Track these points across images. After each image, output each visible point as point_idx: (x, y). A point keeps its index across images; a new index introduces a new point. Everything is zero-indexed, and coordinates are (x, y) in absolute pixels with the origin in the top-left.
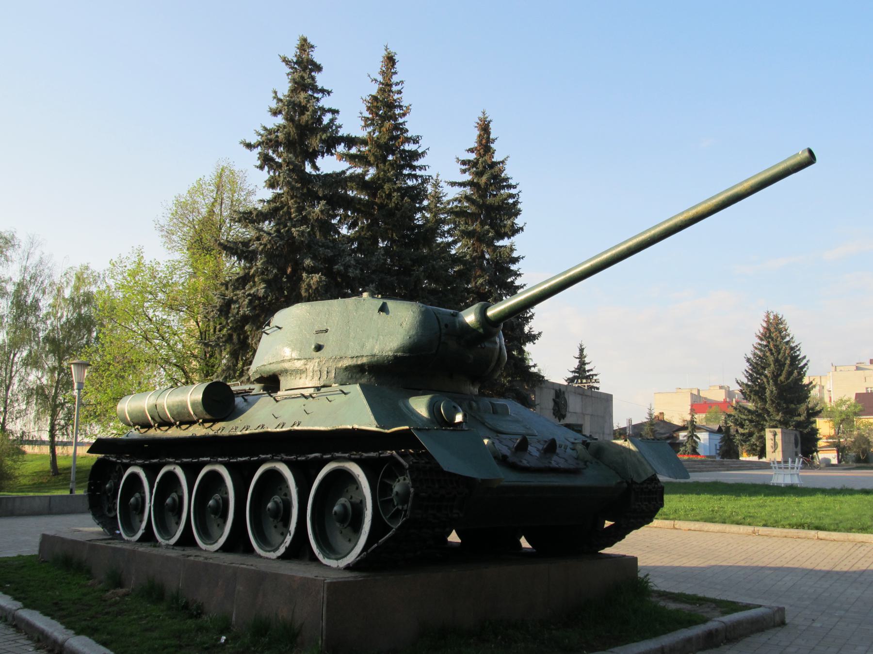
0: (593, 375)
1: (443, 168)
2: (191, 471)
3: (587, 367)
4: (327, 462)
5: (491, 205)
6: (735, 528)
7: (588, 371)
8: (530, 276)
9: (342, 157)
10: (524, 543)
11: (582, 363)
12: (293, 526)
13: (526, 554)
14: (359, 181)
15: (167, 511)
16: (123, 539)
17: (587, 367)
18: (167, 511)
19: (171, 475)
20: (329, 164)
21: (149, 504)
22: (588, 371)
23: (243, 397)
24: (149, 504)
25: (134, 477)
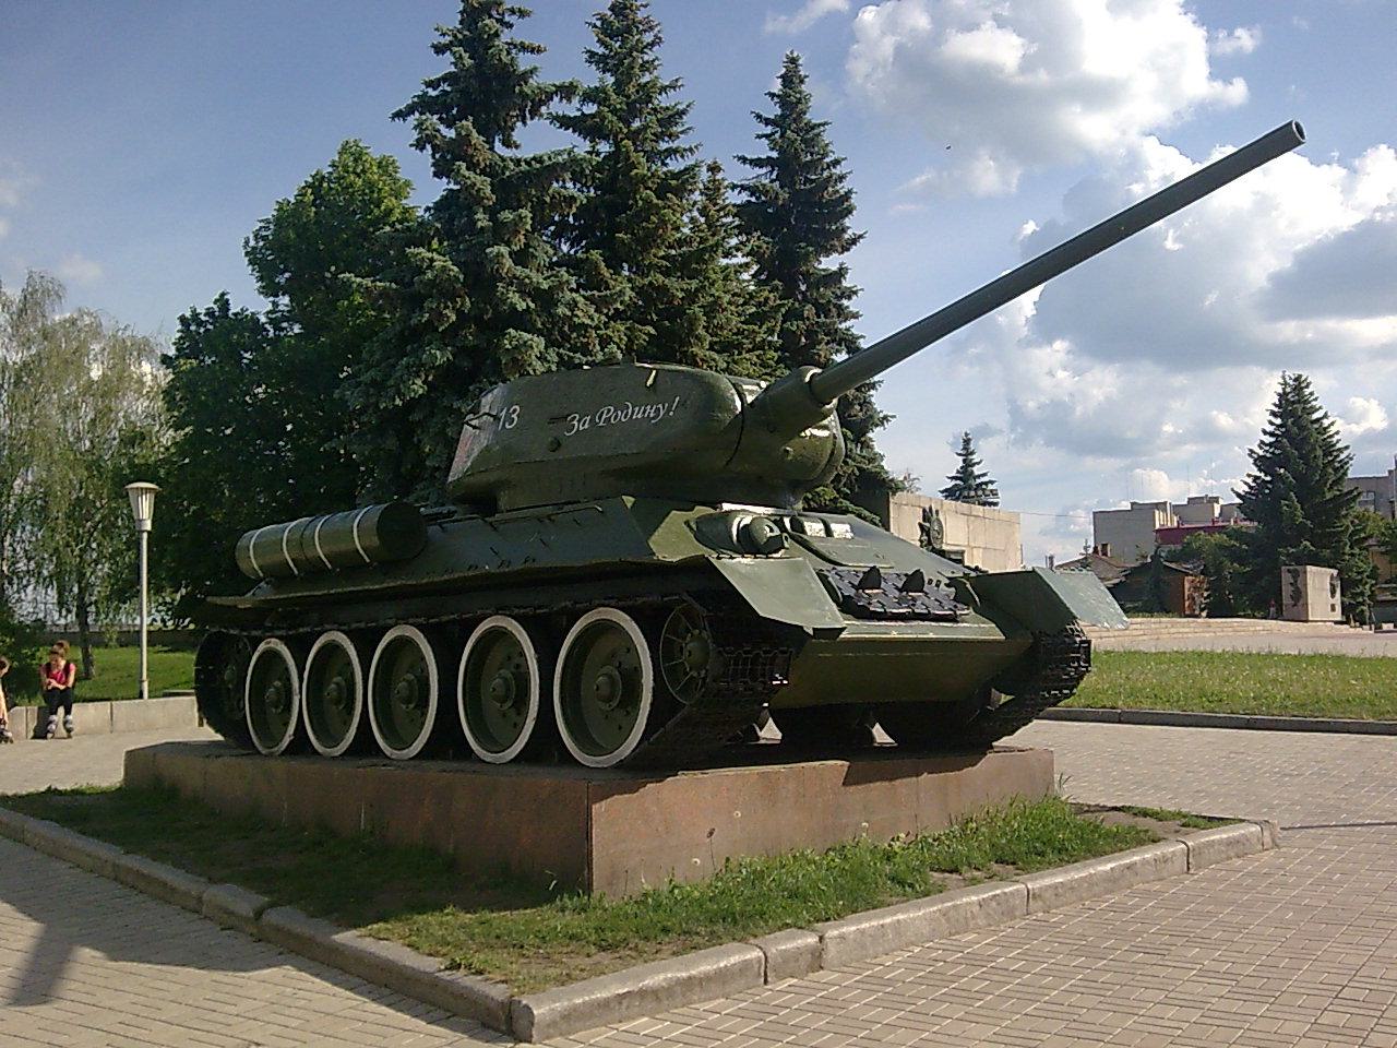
0: (986, 483)
1: (723, 144)
2: (300, 648)
3: (977, 470)
4: (320, 634)
5: (801, 209)
6: (128, 702)
7: (979, 476)
8: (871, 326)
9: (564, 122)
10: (880, 735)
11: (968, 464)
12: (356, 720)
13: (883, 750)
14: (575, 168)
15: (329, 703)
16: (315, 752)
17: (977, 470)
18: (329, 703)
19: (333, 649)
20: (537, 139)
21: (299, 700)
22: (979, 476)
23: (440, 525)
24: (299, 700)
25: (272, 656)
